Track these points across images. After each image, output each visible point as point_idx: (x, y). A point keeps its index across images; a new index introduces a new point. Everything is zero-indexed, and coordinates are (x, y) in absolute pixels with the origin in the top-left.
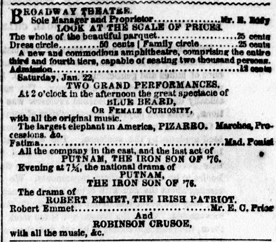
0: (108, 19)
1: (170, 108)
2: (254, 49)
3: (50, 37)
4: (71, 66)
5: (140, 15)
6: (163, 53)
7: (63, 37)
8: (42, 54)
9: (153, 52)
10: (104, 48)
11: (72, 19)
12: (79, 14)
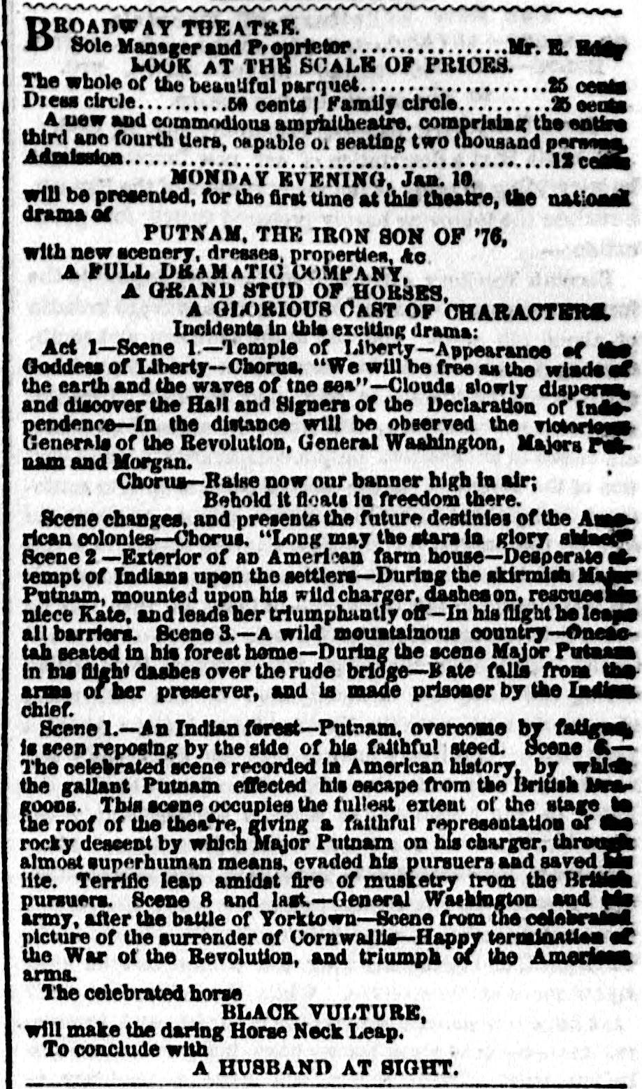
0: (245, 48)
2: (588, 115)
4: (163, 150)
5: (318, 36)
6: (373, 124)
7: (146, 84)
9: (350, 125)
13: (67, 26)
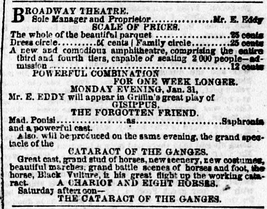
1: (175, 166)
2: (246, 48)
11: (71, 18)
13: (31, 11)
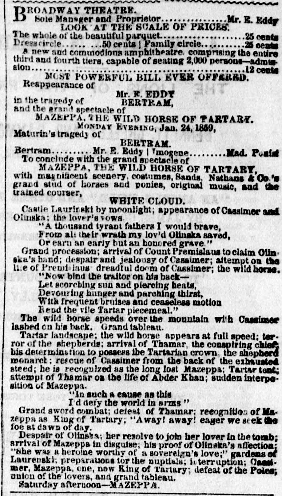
3: (54, 36)
8: (46, 52)
9: (158, 53)
10: (107, 48)
12: (82, 13)
